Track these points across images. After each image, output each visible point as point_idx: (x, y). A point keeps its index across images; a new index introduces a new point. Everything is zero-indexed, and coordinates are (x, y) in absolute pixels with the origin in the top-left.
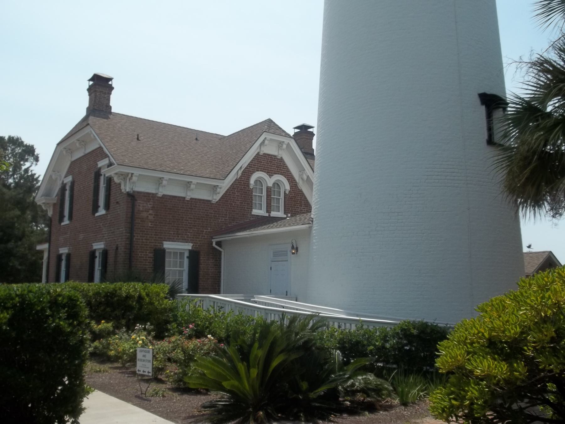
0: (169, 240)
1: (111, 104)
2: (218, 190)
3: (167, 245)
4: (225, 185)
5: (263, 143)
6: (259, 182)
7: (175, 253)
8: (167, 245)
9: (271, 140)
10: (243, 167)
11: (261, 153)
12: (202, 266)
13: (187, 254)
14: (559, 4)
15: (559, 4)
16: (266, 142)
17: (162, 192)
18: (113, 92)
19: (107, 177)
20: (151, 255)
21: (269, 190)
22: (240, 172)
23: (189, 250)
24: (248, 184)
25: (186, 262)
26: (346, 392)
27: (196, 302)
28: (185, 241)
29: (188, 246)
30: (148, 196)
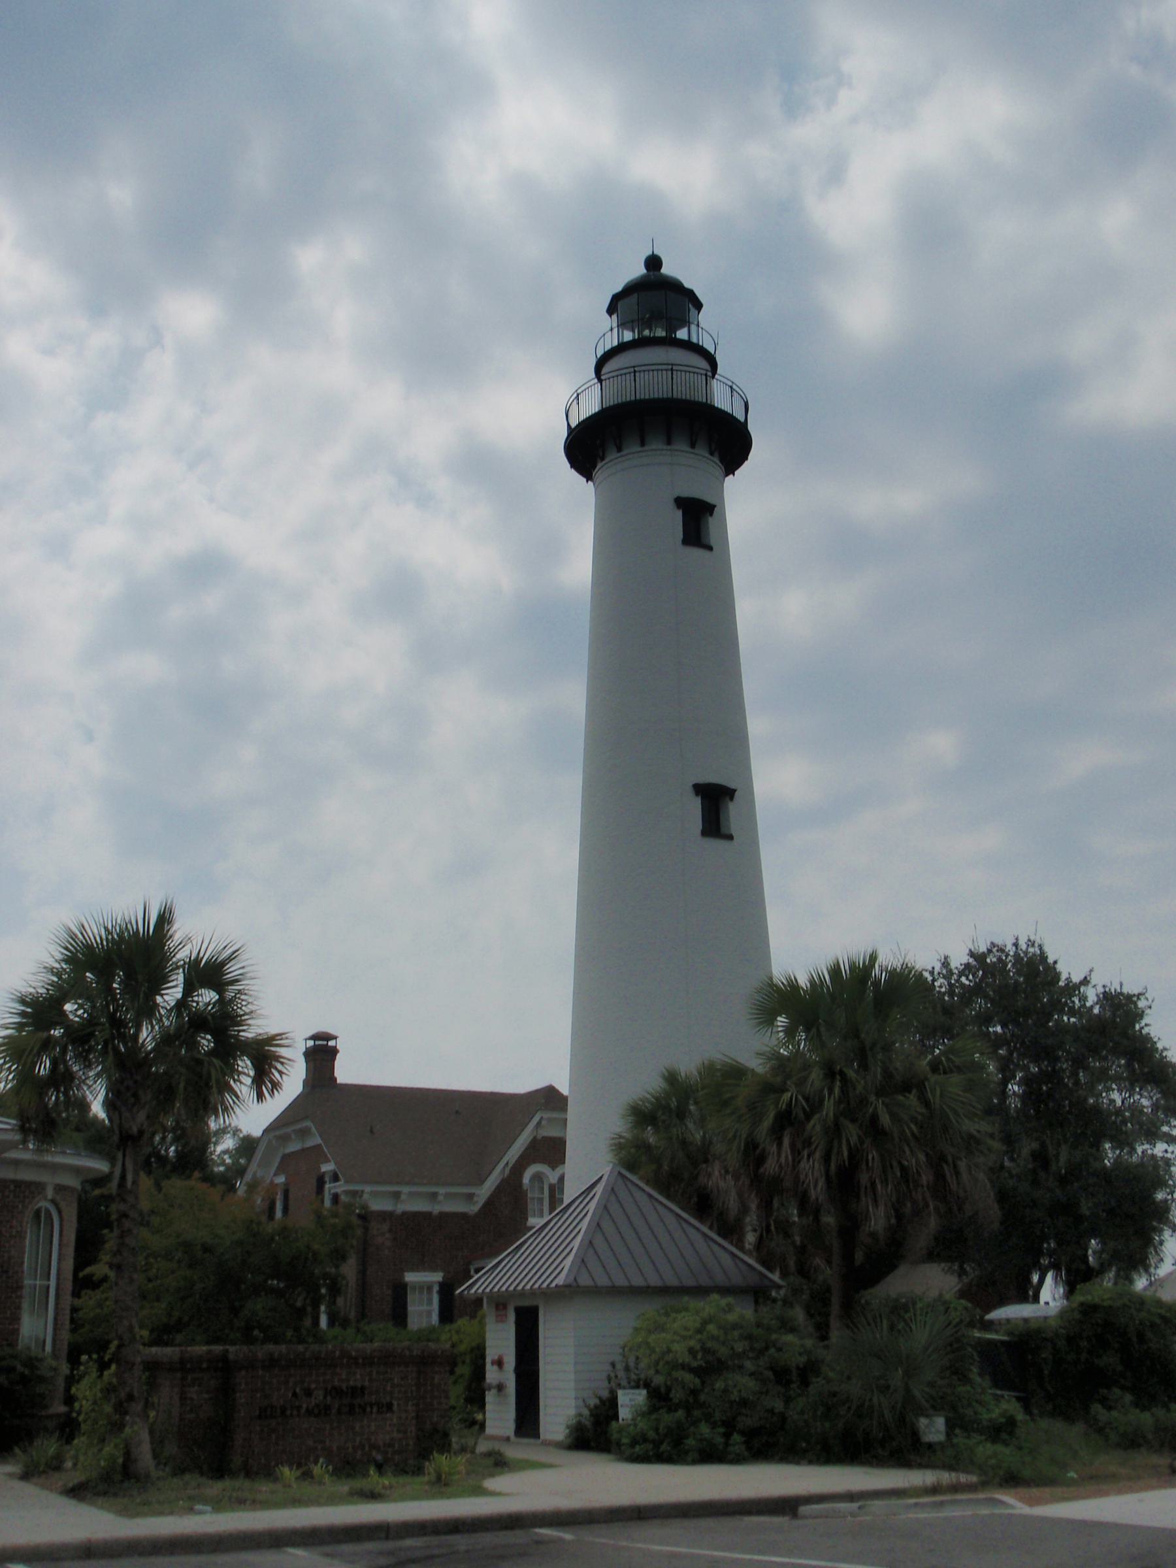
0: (414, 1269)
1: (336, 1075)
2: (475, 1199)
3: (410, 1277)
4: (484, 1191)
5: (539, 1124)
6: (538, 1178)
7: (421, 1288)
8: (410, 1277)
9: (549, 1120)
10: (510, 1162)
11: (539, 1137)
12: (599, 1185)
13: (436, 1288)
14: (82, 942)
15: (82, 942)
16: (543, 1122)
17: (401, 1208)
18: (338, 1056)
19: (333, 1193)
20: (390, 1292)
21: (552, 1188)
22: (507, 1171)
23: (439, 1282)
24: (520, 1184)
25: (436, 1298)
26: (663, 1390)
27: (798, 1042)
28: (433, 1269)
29: (437, 1277)
30: (385, 1216)
